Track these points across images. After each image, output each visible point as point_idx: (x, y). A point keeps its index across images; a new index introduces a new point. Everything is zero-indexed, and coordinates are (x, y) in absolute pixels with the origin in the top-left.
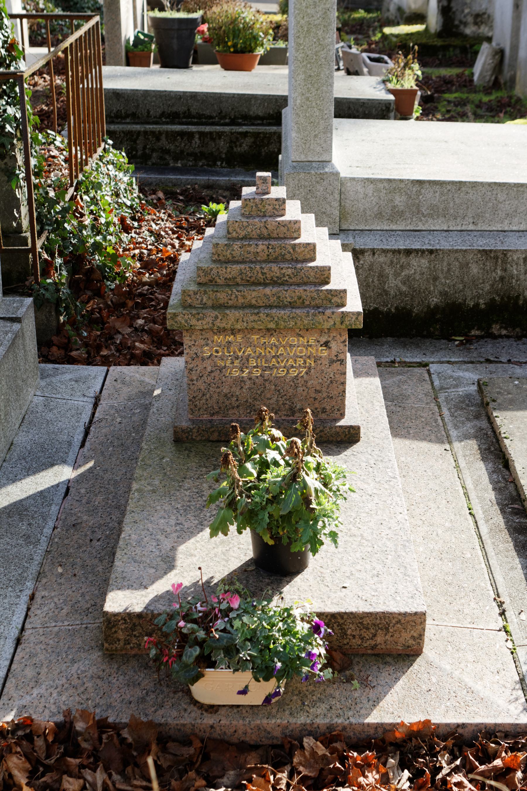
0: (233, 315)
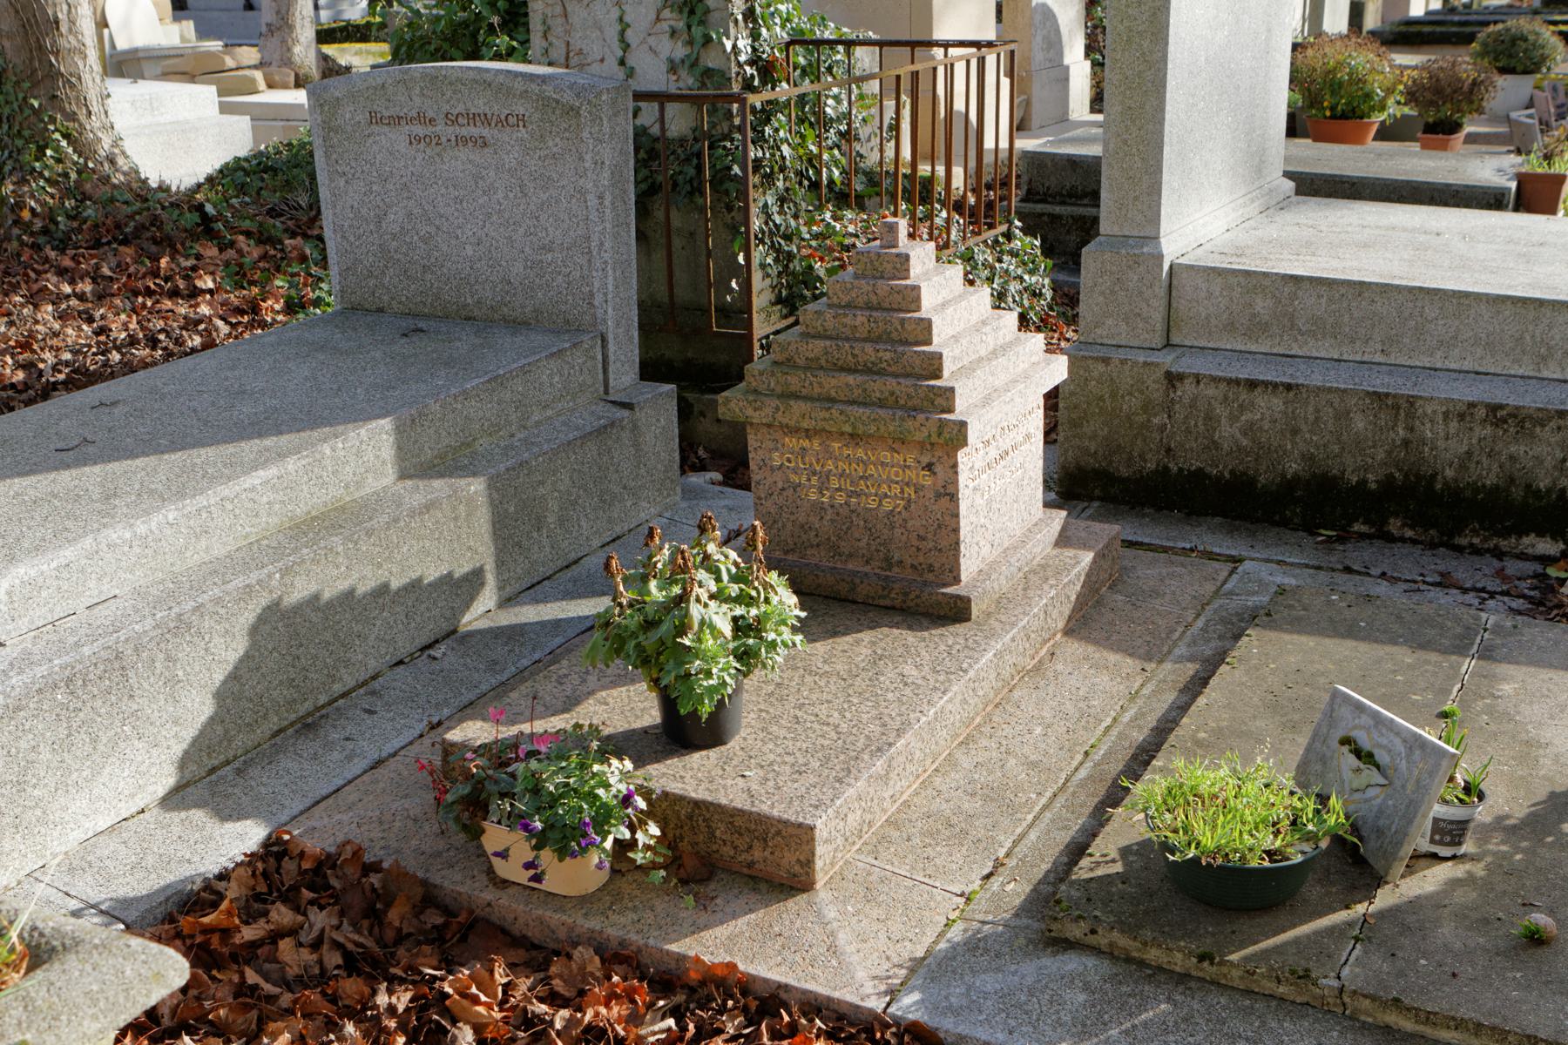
0: (798, 407)
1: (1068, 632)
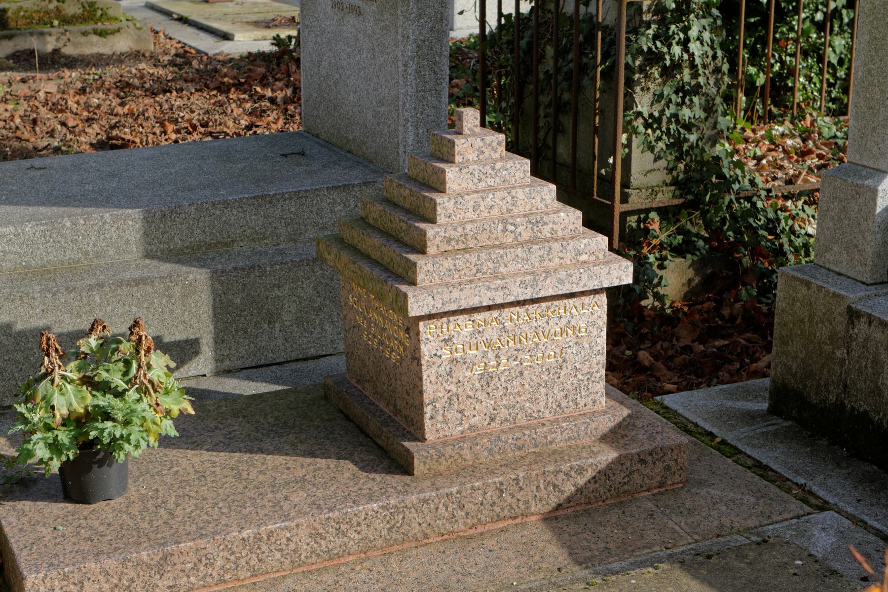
1: (553, 518)
